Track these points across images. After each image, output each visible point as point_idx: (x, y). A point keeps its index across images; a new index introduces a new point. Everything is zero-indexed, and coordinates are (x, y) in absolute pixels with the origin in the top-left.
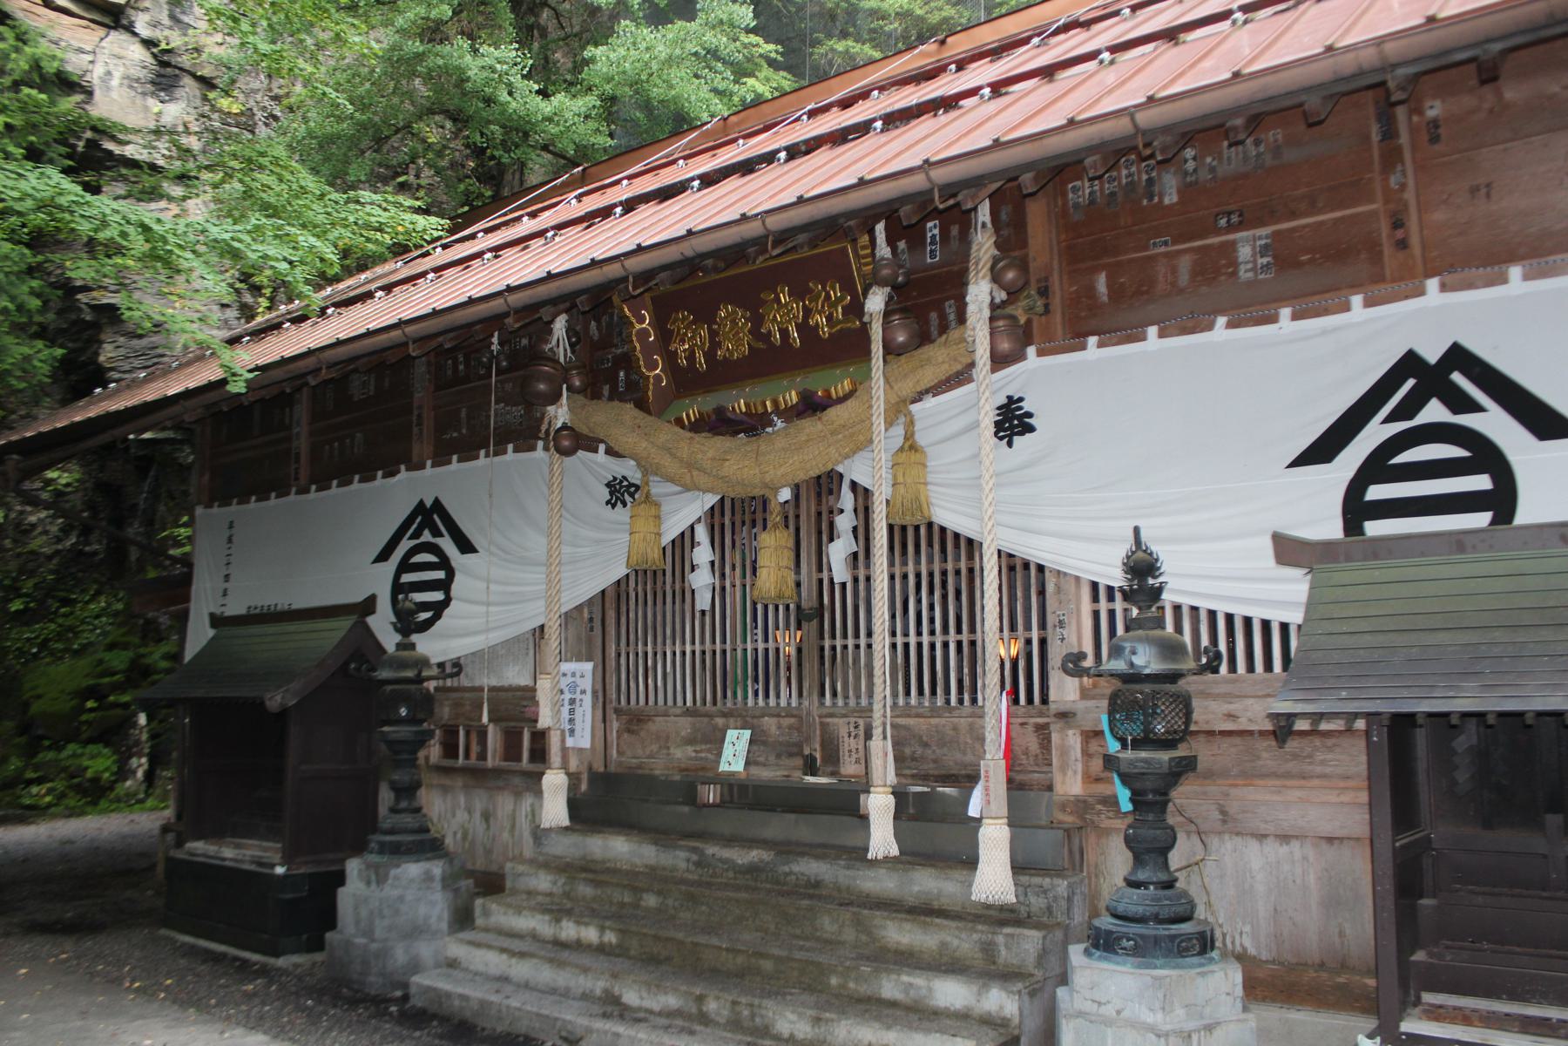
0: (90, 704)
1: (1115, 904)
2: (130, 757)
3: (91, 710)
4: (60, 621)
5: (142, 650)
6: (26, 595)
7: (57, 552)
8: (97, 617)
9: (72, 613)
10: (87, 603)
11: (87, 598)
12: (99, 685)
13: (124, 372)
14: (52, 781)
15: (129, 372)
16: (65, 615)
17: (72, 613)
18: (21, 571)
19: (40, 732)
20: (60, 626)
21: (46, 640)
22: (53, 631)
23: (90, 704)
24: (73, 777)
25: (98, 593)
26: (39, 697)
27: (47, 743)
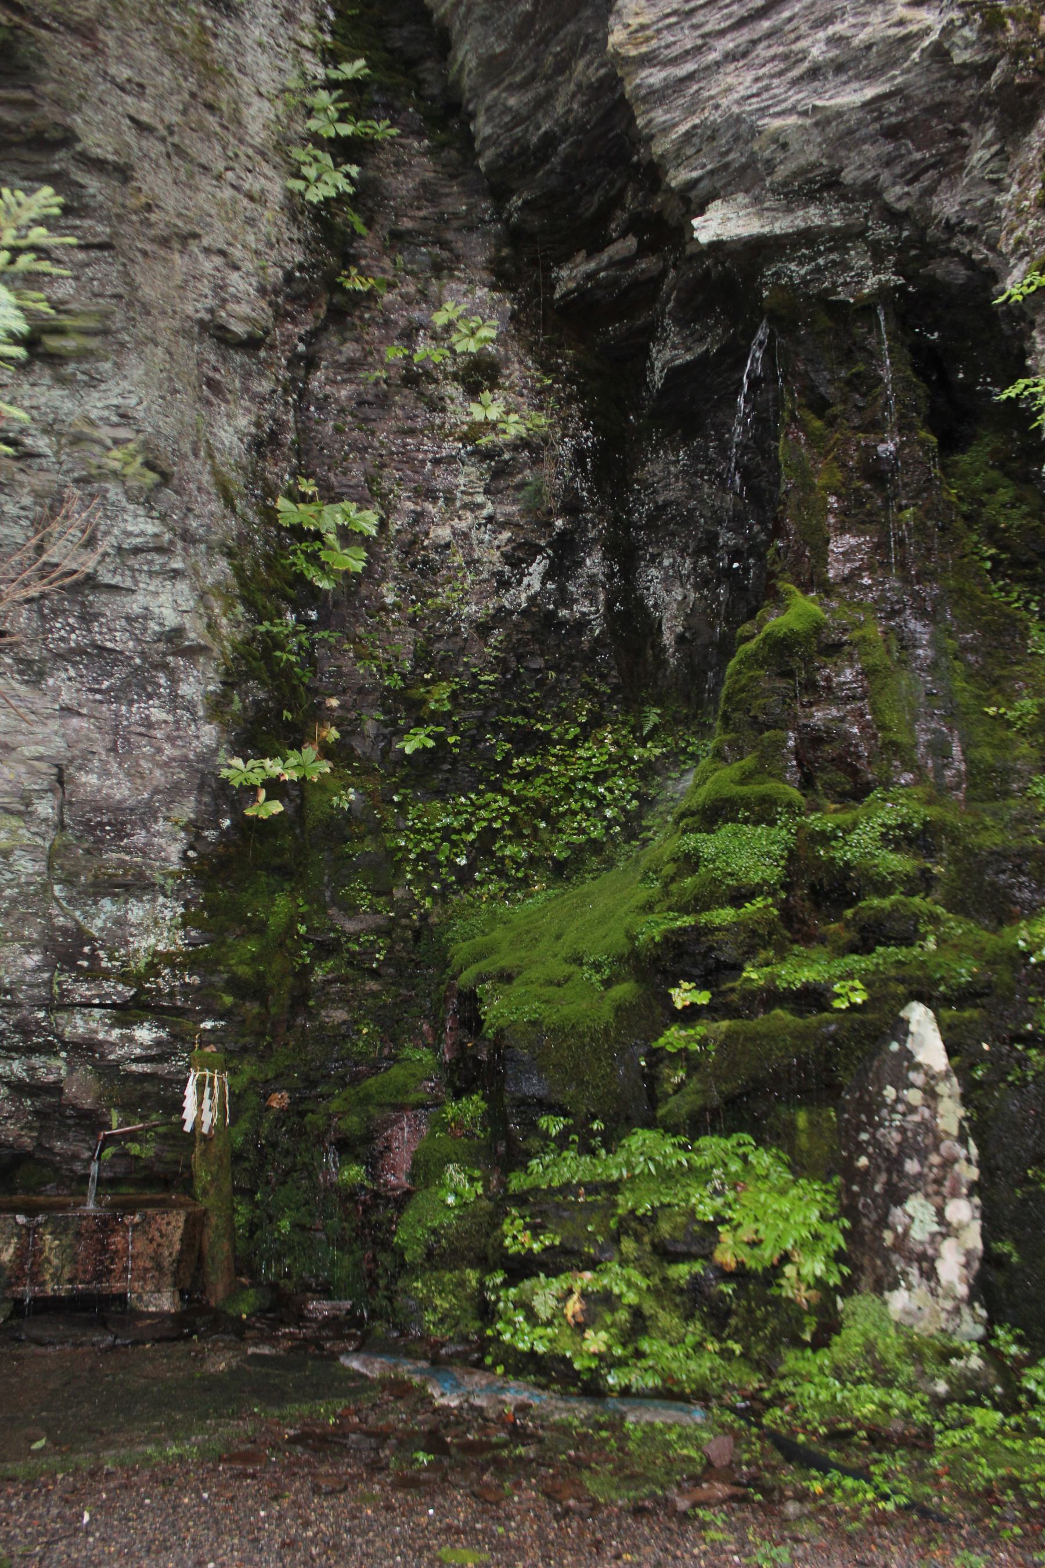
0: (683, 996)
1: (909, 1320)
2: (897, 1196)
3: (691, 1014)
4: (515, 787)
5: (814, 821)
6: (436, 718)
7: (501, 616)
8: (600, 778)
9: (539, 770)
10: (573, 744)
11: (574, 731)
12: (700, 931)
13: (675, 61)
14: (592, 1264)
15: (697, 50)
16: (525, 775)
17: (539, 770)
18: (423, 658)
19: (533, 1087)
20: (515, 801)
21: (490, 835)
22: (503, 812)
23: (683, 996)
24: (672, 1257)
25: (596, 721)
26: (506, 977)
27: (553, 1125)
